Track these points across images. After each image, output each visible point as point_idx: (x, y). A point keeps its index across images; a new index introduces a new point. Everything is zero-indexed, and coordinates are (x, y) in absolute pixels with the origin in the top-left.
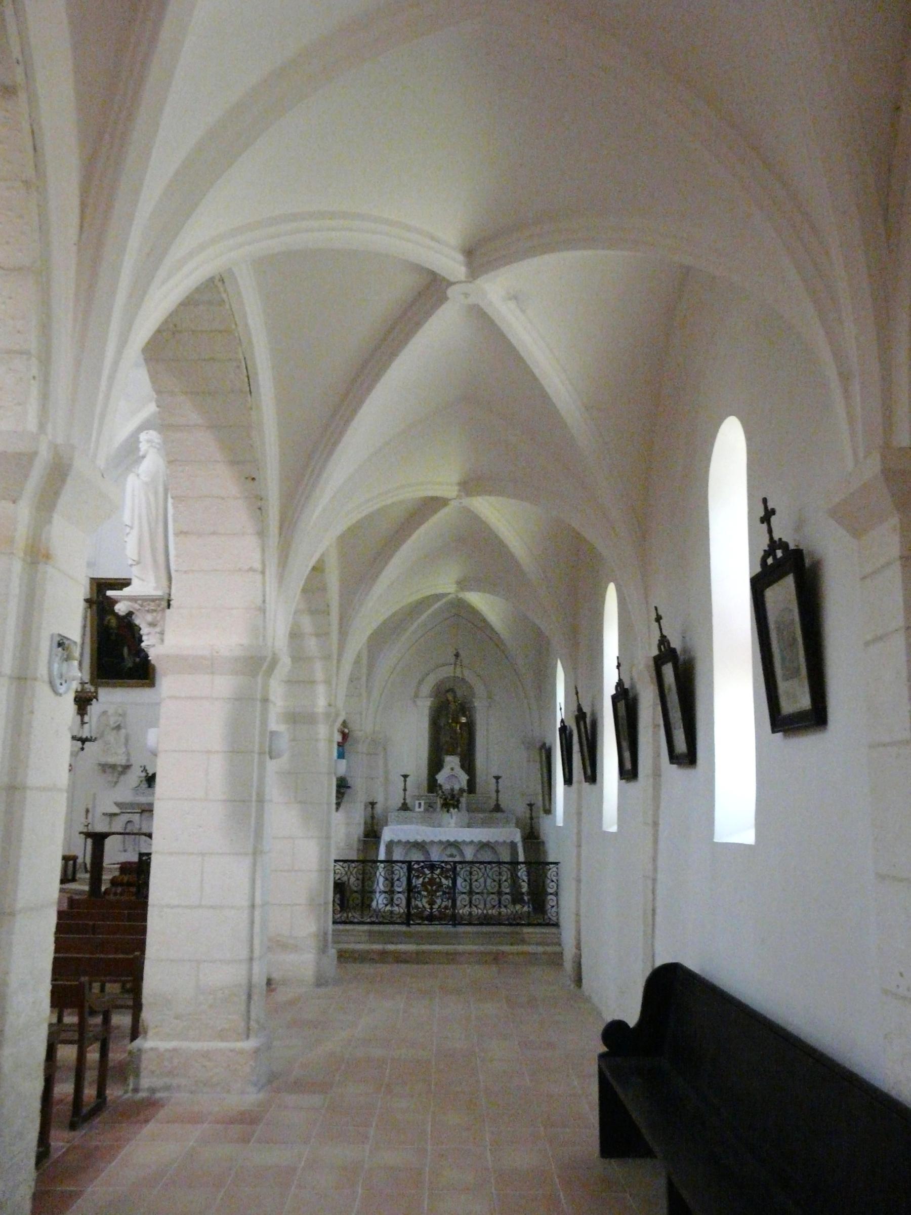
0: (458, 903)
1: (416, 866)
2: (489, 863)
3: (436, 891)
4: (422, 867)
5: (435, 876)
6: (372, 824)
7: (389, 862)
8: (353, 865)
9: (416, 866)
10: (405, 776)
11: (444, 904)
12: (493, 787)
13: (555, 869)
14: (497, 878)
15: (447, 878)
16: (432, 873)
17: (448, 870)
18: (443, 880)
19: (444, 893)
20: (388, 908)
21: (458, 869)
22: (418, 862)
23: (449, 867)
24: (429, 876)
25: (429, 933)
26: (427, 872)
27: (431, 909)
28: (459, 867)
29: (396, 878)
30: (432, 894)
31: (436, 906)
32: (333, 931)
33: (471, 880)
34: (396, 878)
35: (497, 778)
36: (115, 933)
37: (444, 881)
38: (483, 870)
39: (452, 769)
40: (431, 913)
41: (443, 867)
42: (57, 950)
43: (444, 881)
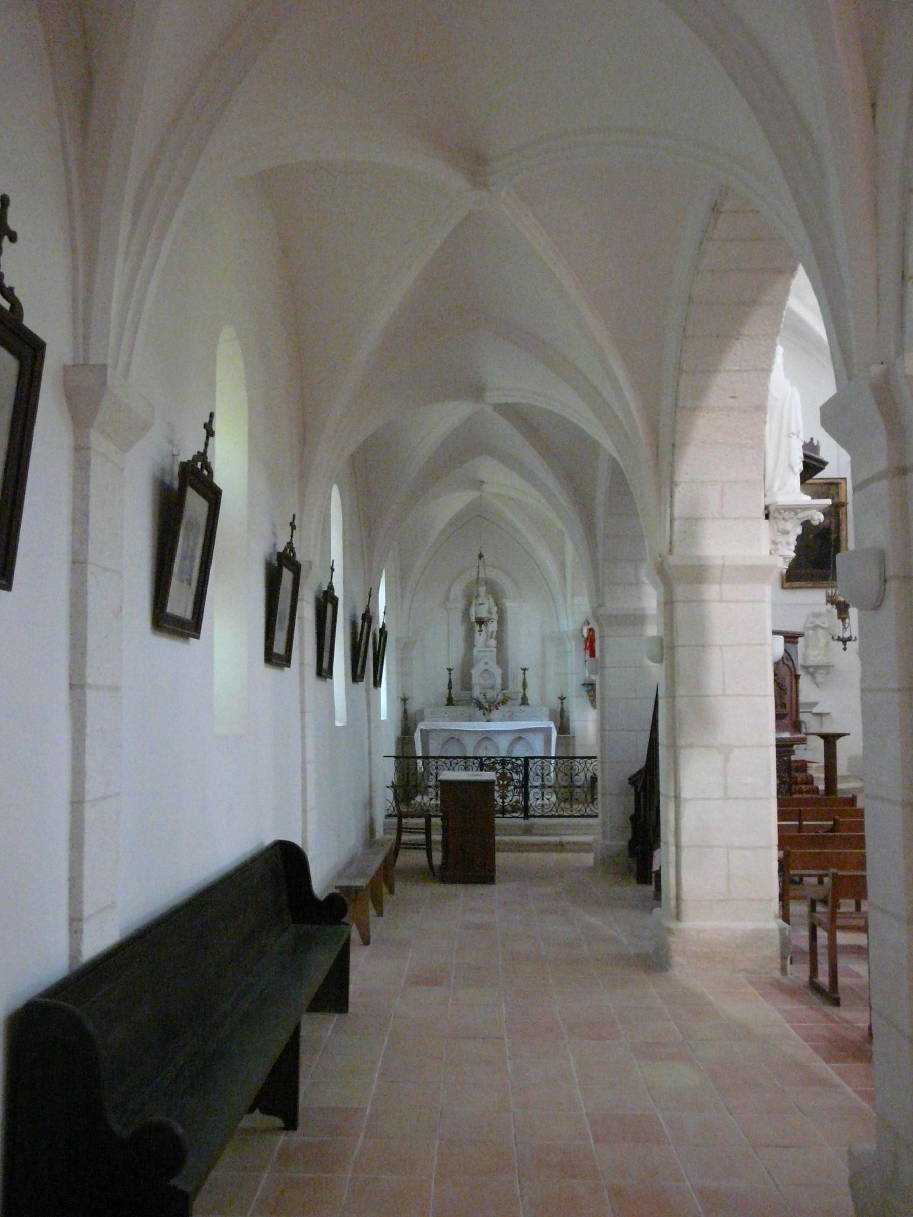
0: (531, 796)
1: (487, 762)
2: (455, 758)
3: (508, 785)
4: (493, 763)
5: (506, 771)
6: (562, 723)
7: (425, 758)
8: (455, 761)
9: (487, 762)
10: (450, 670)
11: (515, 798)
12: (521, 677)
13: (434, 763)
14: (568, 773)
15: (517, 773)
16: (503, 768)
17: (519, 766)
18: (514, 775)
19: (516, 787)
20: (539, 802)
21: (530, 765)
22: (489, 758)
23: (519, 762)
24: (500, 771)
25: (568, 825)
26: (498, 767)
27: (503, 802)
28: (531, 762)
29: (546, 773)
30: (504, 788)
31: (507, 800)
32: (385, 824)
33: (543, 774)
34: (546, 773)
35: (525, 670)
36: (789, 806)
37: (515, 776)
38: (583, 765)
39: (486, 663)
40: (503, 807)
41: (513, 763)
42: (781, 816)
43: (515, 776)
